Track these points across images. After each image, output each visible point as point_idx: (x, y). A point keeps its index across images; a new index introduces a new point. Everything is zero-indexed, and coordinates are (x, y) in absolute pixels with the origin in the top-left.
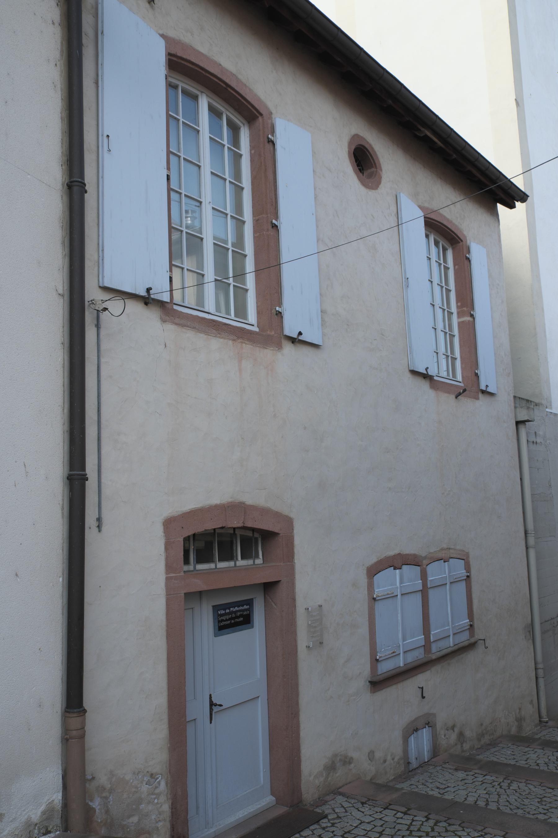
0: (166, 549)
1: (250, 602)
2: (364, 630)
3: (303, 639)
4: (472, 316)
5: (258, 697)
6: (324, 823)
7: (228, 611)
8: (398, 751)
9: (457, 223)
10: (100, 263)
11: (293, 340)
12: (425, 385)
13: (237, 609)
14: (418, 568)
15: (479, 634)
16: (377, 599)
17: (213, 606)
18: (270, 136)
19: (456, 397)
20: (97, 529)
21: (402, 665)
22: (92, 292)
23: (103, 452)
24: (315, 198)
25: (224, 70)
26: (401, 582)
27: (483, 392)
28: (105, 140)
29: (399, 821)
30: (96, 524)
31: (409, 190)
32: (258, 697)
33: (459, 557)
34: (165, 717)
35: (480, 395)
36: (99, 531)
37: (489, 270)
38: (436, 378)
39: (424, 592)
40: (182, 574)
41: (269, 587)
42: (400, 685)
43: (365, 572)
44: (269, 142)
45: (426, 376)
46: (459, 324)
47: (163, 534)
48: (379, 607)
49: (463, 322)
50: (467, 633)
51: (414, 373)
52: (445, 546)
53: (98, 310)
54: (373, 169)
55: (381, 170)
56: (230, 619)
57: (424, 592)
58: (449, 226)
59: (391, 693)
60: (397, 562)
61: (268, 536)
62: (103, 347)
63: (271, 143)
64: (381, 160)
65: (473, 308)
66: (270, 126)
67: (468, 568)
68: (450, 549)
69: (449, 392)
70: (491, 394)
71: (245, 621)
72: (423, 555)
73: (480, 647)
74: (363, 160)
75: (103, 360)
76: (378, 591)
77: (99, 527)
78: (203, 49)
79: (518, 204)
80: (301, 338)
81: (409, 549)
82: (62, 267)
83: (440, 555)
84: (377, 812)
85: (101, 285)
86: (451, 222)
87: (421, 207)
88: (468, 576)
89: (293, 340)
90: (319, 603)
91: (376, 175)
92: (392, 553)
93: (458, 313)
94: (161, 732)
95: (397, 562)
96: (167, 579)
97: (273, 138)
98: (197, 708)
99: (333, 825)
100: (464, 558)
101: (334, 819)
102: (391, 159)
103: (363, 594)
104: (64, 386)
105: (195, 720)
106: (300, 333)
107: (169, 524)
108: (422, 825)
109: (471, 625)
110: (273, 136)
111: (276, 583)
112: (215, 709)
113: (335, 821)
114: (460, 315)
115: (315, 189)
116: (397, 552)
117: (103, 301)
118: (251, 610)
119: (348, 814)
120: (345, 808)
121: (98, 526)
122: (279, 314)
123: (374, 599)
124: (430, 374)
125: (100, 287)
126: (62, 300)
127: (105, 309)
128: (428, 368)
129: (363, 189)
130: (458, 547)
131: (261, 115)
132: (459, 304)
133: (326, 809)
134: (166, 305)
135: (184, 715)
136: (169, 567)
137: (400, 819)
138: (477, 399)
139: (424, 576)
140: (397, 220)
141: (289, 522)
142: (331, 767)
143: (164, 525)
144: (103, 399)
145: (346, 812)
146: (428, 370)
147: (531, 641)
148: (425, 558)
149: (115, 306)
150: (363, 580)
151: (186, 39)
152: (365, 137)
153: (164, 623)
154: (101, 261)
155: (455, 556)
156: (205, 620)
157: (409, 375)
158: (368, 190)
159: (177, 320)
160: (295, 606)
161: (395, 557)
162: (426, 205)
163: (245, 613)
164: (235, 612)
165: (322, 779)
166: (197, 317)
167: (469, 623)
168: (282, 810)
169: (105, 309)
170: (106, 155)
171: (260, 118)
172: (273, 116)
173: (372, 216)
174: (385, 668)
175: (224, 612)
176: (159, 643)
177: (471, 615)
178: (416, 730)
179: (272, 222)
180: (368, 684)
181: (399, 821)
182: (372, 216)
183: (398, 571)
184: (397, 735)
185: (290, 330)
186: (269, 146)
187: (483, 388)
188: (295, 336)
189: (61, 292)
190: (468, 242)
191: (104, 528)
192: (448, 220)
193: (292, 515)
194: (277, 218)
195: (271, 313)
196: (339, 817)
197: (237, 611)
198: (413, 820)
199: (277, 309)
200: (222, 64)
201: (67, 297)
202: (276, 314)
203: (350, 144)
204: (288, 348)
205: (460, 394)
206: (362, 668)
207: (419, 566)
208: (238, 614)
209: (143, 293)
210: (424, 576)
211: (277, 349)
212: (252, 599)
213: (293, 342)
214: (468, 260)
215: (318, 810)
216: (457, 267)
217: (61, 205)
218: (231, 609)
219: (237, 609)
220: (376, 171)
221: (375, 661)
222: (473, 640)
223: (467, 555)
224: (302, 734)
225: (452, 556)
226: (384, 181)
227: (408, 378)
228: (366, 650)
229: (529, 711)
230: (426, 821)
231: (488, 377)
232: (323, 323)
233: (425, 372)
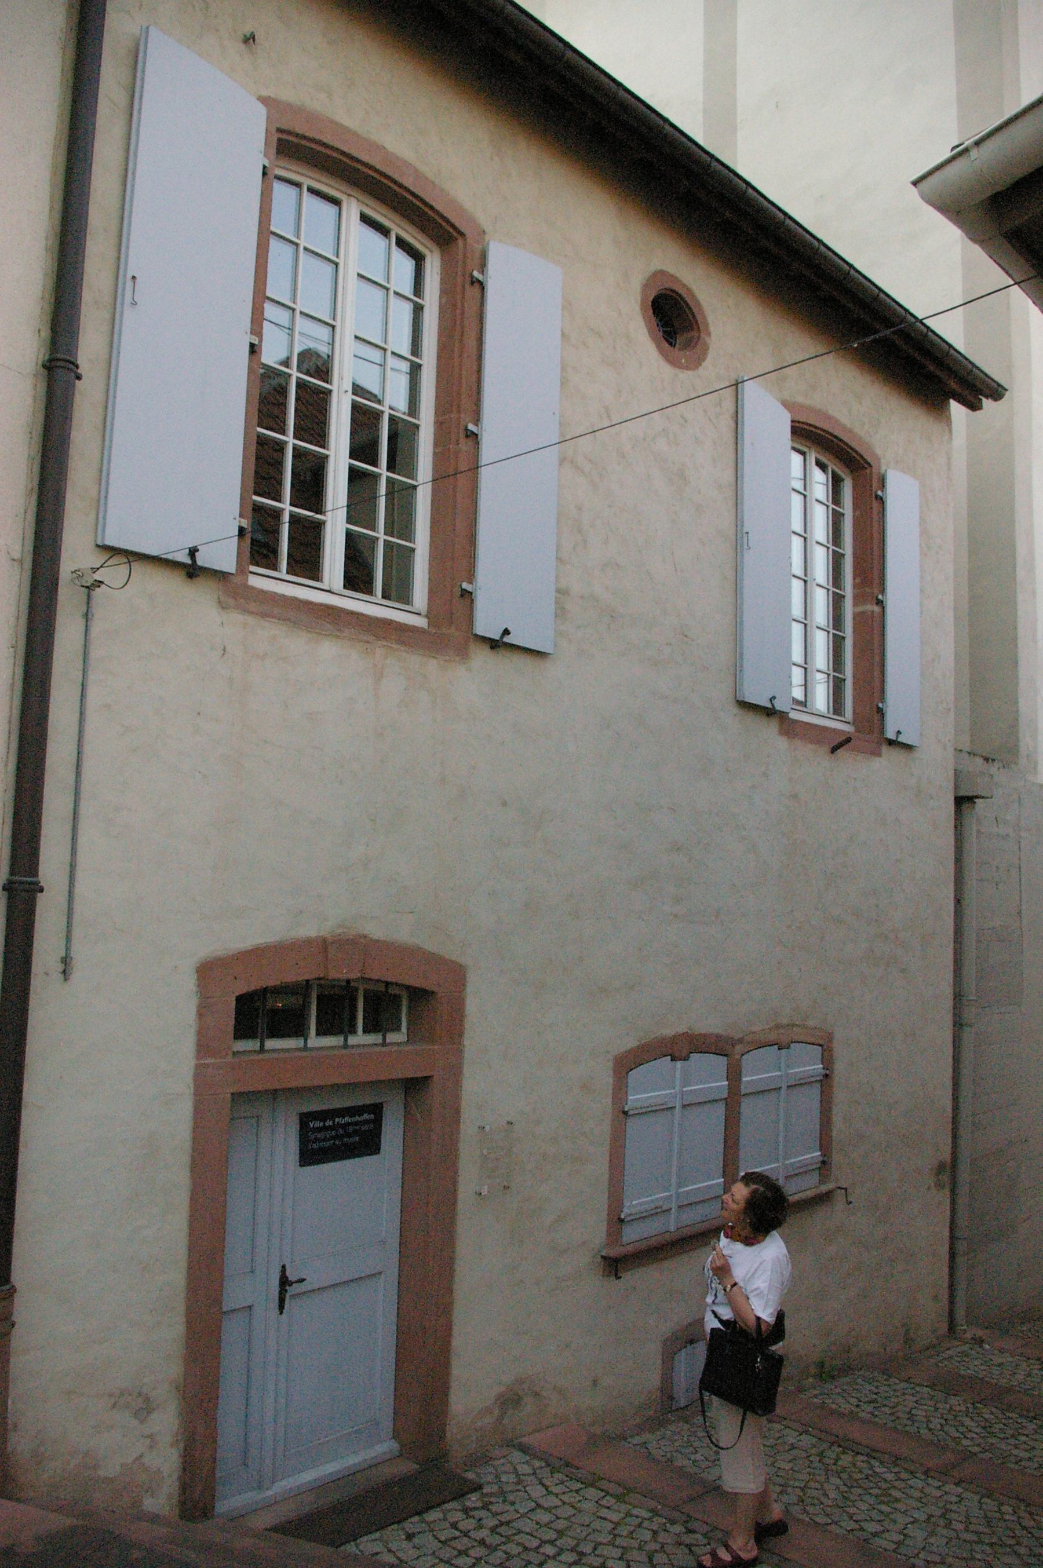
0: (200, 1015)
1: (377, 1109)
2: (599, 1167)
3: (469, 1180)
4: (880, 603)
5: (380, 1273)
6: (473, 1500)
7: (329, 1123)
8: (653, 1379)
9: (862, 434)
10: (99, 504)
11: (494, 645)
12: (770, 729)
13: (347, 1119)
14: (723, 1061)
15: (841, 1175)
16: (630, 1113)
17: (305, 1119)
18: (476, 274)
19: (832, 752)
20: (62, 976)
21: (672, 1228)
22: (76, 554)
23: (82, 840)
24: (562, 384)
25: (390, 158)
26: (686, 1082)
27: (891, 743)
28: (129, 284)
29: (604, 1513)
30: (61, 967)
31: (764, 361)
32: (380, 1273)
33: (813, 1040)
34: (181, 1307)
35: (885, 749)
36: (66, 980)
37: (923, 521)
38: (793, 715)
39: (733, 1100)
40: (229, 1058)
41: (414, 1087)
42: (667, 1264)
43: (611, 1064)
44: (472, 283)
45: (769, 712)
46: (856, 616)
47: (195, 989)
48: (633, 1127)
49: (863, 613)
50: (815, 1177)
51: (745, 706)
52: (785, 1021)
53: (87, 587)
54: (695, 334)
55: (709, 334)
56: (333, 1138)
57: (733, 1100)
58: (845, 439)
59: (643, 1279)
60: (681, 1048)
61: (419, 996)
62: (95, 653)
63: (476, 285)
64: (711, 318)
65: (883, 591)
66: (478, 254)
67: (827, 1059)
68: (793, 1025)
69: (818, 742)
70: (908, 747)
71: (367, 1143)
72: (737, 1036)
73: (839, 1203)
74: (672, 318)
75: (92, 677)
76: (635, 1099)
77: (65, 973)
78: (845, 420)
79: (986, 403)
80: (506, 639)
81: (710, 1024)
82: (22, 511)
83: (772, 1037)
84: (571, 1491)
85: (99, 543)
86: (850, 431)
87: (785, 404)
88: (826, 1076)
89: (494, 645)
90: (509, 1119)
91: (696, 343)
92: (668, 1032)
93: (856, 597)
94: (173, 1330)
95: (681, 1048)
96: (198, 1066)
97: (480, 277)
98: (248, 1288)
99: (485, 1507)
100: (821, 1042)
101: (491, 1495)
102: (733, 315)
103: (605, 1102)
104: (10, 722)
105: (250, 1307)
106: (506, 632)
107: (208, 971)
108: (640, 1525)
109: (823, 1162)
110: (482, 272)
111: (427, 1079)
112: (291, 1290)
113: (492, 1499)
114: (858, 599)
115: (563, 368)
116: (682, 1029)
117: (95, 570)
118: (378, 1122)
119: (520, 1487)
120: (517, 1475)
121: (64, 972)
122: (467, 596)
123: (625, 1113)
124: (777, 708)
125: (98, 546)
126: (17, 571)
127: (100, 583)
128: (774, 698)
129: (667, 370)
130: (811, 1023)
131: (462, 234)
132: (858, 580)
133: (486, 1475)
134: (231, 577)
135: (218, 1301)
136: (203, 1048)
137: (606, 1510)
138: (879, 755)
139: (734, 1075)
140: (733, 425)
141: (457, 974)
142: (510, 1400)
143: (197, 972)
144: (87, 749)
145: (518, 1483)
146: (775, 702)
147: (947, 1192)
148: (741, 1041)
149: (114, 574)
150: (606, 1079)
151: (317, 103)
152: (678, 275)
153: (188, 1144)
154: (102, 501)
155: (802, 1038)
156: (283, 1139)
157: (736, 710)
158: (677, 371)
159: (252, 606)
160: (458, 1122)
161: (675, 1039)
162: (800, 399)
163: (365, 1128)
164: (344, 1126)
165: (488, 1420)
166: (295, 599)
167: (821, 1159)
168: (408, 1467)
169: (100, 583)
170: (128, 312)
171: (460, 242)
172: (487, 238)
173: (682, 417)
174: (633, 1235)
175: (321, 1124)
176: (176, 1175)
177: (825, 1143)
178: (692, 1342)
179: (466, 427)
180: (599, 1259)
181: (604, 1513)
182: (682, 417)
183: (679, 1064)
184: (653, 1350)
185: (486, 625)
186: (473, 292)
187: (890, 734)
188: (496, 636)
189: (17, 555)
190: (883, 468)
191: (76, 975)
192: (844, 428)
193: (465, 960)
194: (477, 421)
195: (455, 599)
196: (502, 1493)
197: (349, 1124)
198: (628, 1514)
199: (465, 585)
200: (387, 146)
201: (28, 565)
202: (462, 596)
203: (645, 287)
204: (481, 657)
205: (840, 745)
206: (590, 1231)
207: (725, 1055)
208: (351, 1129)
209: (184, 558)
210: (734, 1075)
211: (457, 658)
212: (381, 1104)
213: (492, 648)
214: (881, 501)
215: (470, 1476)
216: (858, 513)
217: (30, 401)
218: (337, 1120)
219: (347, 1119)
220: (699, 337)
221: (617, 1222)
222: (824, 1188)
223: (830, 1037)
224: (456, 1342)
225: (796, 1038)
226: (707, 363)
227: (731, 716)
228: (601, 1201)
229: (930, 1313)
230: (822, 1452)
231: (901, 715)
232: (561, 613)
233: (769, 706)
